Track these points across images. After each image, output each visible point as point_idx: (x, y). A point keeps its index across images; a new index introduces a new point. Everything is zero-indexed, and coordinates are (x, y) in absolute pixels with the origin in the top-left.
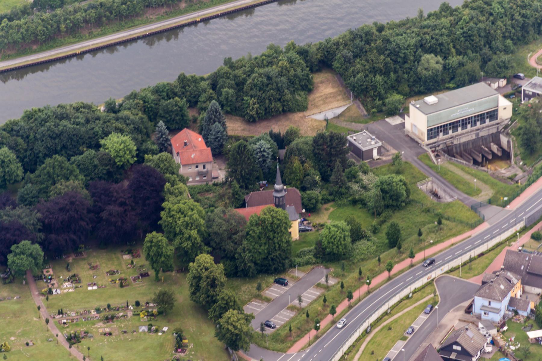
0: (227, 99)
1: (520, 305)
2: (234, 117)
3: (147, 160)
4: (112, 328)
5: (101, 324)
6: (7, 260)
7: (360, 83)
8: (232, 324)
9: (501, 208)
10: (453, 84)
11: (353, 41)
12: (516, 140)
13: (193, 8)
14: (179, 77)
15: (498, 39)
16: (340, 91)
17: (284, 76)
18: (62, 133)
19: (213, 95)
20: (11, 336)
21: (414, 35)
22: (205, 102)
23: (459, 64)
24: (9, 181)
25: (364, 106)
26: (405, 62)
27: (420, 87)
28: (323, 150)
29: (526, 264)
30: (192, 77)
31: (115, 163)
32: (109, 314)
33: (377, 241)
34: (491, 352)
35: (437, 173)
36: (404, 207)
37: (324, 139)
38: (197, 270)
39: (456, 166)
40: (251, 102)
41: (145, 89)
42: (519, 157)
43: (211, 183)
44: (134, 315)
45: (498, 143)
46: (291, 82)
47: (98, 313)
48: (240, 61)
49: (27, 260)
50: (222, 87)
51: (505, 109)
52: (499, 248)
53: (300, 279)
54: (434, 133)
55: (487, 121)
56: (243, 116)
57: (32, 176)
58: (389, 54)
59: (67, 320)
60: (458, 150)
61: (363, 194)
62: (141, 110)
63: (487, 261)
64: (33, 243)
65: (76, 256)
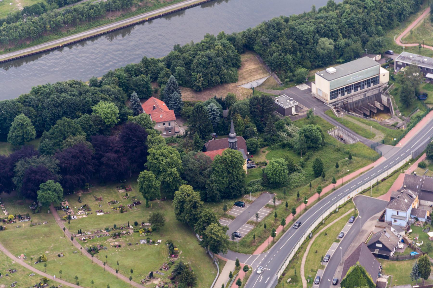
0: (179, 75)
1: (420, 214)
2: (185, 88)
3: (130, 119)
4: (120, 242)
5: (111, 239)
6: (37, 195)
7: (276, 60)
8: (214, 234)
9: (393, 146)
10: (342, 59)
11: (268, 30)
12: (394, 98)
13: (142, 11)
14: (143, 60)
15: (372, 26)
16: (261, 67)
17: (220, 56)
18: (63, 102)
19: (169, 72)
20: (46, 250)
21: (312, 24)
22: (163, 77)
23: (346, 44)
24: (26, 139)
25: (279, 78)
26: (307, 44)
27: (319, 62)
28: (257, 108)
29: (420, 184)
30: (152, 59)
31: (105, 123)
32: (117, 232)
33: (305, 173)
34: (403, 248)
35: (341, 123)
36: (321, 149)
37: (258, 100)
38: (181, 196)
39: (353, 118)
40: (198, 76)
41: (118, 70)
42: (398, 110)
43: (175, 136)
44: (134, 232)
45: (380, 101)
46: (226, 61)
47: (107, 232)
48: (185, 46)
49: (53, 194)
50: (176, 66)
51: (384, 75)
52: (396, 175)
53: (253, 202)
54: (335, 94)
55: (372, 84)
56: (191, 87)
57: (47, 133)
58: (295, 38)
59: (85, 237)
60: (352, 107)
61: (289, 140)
62: (117, 84)
63: (388, 184)
64: (55, 182)
65: (84, 192)
